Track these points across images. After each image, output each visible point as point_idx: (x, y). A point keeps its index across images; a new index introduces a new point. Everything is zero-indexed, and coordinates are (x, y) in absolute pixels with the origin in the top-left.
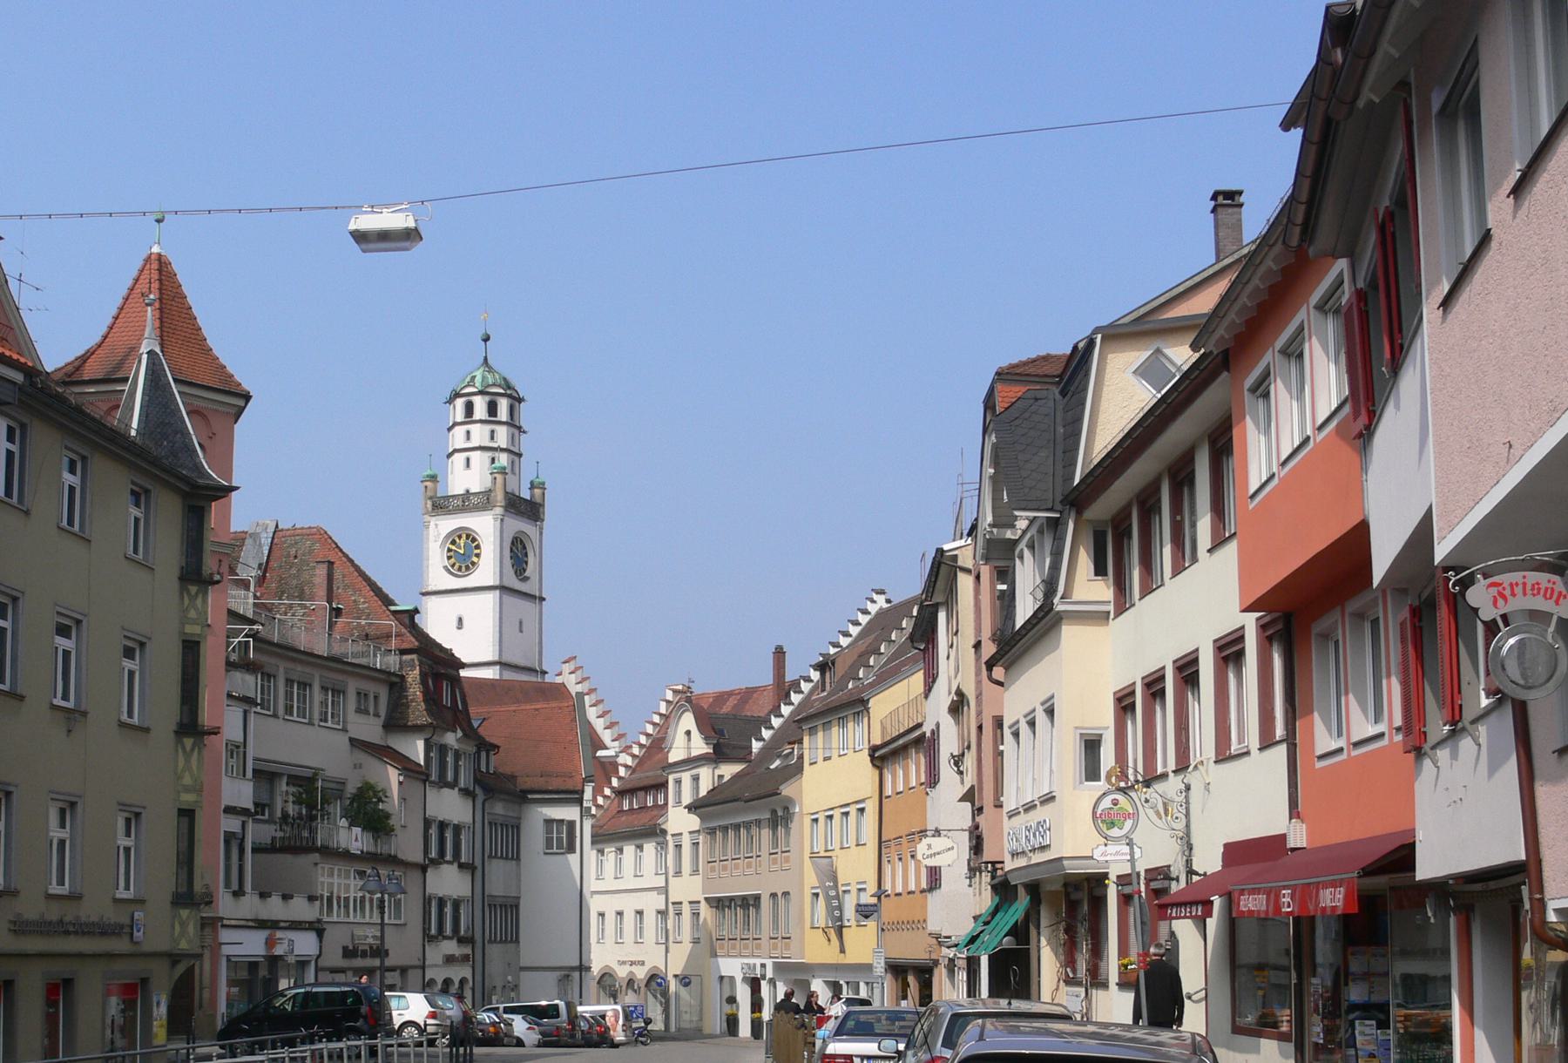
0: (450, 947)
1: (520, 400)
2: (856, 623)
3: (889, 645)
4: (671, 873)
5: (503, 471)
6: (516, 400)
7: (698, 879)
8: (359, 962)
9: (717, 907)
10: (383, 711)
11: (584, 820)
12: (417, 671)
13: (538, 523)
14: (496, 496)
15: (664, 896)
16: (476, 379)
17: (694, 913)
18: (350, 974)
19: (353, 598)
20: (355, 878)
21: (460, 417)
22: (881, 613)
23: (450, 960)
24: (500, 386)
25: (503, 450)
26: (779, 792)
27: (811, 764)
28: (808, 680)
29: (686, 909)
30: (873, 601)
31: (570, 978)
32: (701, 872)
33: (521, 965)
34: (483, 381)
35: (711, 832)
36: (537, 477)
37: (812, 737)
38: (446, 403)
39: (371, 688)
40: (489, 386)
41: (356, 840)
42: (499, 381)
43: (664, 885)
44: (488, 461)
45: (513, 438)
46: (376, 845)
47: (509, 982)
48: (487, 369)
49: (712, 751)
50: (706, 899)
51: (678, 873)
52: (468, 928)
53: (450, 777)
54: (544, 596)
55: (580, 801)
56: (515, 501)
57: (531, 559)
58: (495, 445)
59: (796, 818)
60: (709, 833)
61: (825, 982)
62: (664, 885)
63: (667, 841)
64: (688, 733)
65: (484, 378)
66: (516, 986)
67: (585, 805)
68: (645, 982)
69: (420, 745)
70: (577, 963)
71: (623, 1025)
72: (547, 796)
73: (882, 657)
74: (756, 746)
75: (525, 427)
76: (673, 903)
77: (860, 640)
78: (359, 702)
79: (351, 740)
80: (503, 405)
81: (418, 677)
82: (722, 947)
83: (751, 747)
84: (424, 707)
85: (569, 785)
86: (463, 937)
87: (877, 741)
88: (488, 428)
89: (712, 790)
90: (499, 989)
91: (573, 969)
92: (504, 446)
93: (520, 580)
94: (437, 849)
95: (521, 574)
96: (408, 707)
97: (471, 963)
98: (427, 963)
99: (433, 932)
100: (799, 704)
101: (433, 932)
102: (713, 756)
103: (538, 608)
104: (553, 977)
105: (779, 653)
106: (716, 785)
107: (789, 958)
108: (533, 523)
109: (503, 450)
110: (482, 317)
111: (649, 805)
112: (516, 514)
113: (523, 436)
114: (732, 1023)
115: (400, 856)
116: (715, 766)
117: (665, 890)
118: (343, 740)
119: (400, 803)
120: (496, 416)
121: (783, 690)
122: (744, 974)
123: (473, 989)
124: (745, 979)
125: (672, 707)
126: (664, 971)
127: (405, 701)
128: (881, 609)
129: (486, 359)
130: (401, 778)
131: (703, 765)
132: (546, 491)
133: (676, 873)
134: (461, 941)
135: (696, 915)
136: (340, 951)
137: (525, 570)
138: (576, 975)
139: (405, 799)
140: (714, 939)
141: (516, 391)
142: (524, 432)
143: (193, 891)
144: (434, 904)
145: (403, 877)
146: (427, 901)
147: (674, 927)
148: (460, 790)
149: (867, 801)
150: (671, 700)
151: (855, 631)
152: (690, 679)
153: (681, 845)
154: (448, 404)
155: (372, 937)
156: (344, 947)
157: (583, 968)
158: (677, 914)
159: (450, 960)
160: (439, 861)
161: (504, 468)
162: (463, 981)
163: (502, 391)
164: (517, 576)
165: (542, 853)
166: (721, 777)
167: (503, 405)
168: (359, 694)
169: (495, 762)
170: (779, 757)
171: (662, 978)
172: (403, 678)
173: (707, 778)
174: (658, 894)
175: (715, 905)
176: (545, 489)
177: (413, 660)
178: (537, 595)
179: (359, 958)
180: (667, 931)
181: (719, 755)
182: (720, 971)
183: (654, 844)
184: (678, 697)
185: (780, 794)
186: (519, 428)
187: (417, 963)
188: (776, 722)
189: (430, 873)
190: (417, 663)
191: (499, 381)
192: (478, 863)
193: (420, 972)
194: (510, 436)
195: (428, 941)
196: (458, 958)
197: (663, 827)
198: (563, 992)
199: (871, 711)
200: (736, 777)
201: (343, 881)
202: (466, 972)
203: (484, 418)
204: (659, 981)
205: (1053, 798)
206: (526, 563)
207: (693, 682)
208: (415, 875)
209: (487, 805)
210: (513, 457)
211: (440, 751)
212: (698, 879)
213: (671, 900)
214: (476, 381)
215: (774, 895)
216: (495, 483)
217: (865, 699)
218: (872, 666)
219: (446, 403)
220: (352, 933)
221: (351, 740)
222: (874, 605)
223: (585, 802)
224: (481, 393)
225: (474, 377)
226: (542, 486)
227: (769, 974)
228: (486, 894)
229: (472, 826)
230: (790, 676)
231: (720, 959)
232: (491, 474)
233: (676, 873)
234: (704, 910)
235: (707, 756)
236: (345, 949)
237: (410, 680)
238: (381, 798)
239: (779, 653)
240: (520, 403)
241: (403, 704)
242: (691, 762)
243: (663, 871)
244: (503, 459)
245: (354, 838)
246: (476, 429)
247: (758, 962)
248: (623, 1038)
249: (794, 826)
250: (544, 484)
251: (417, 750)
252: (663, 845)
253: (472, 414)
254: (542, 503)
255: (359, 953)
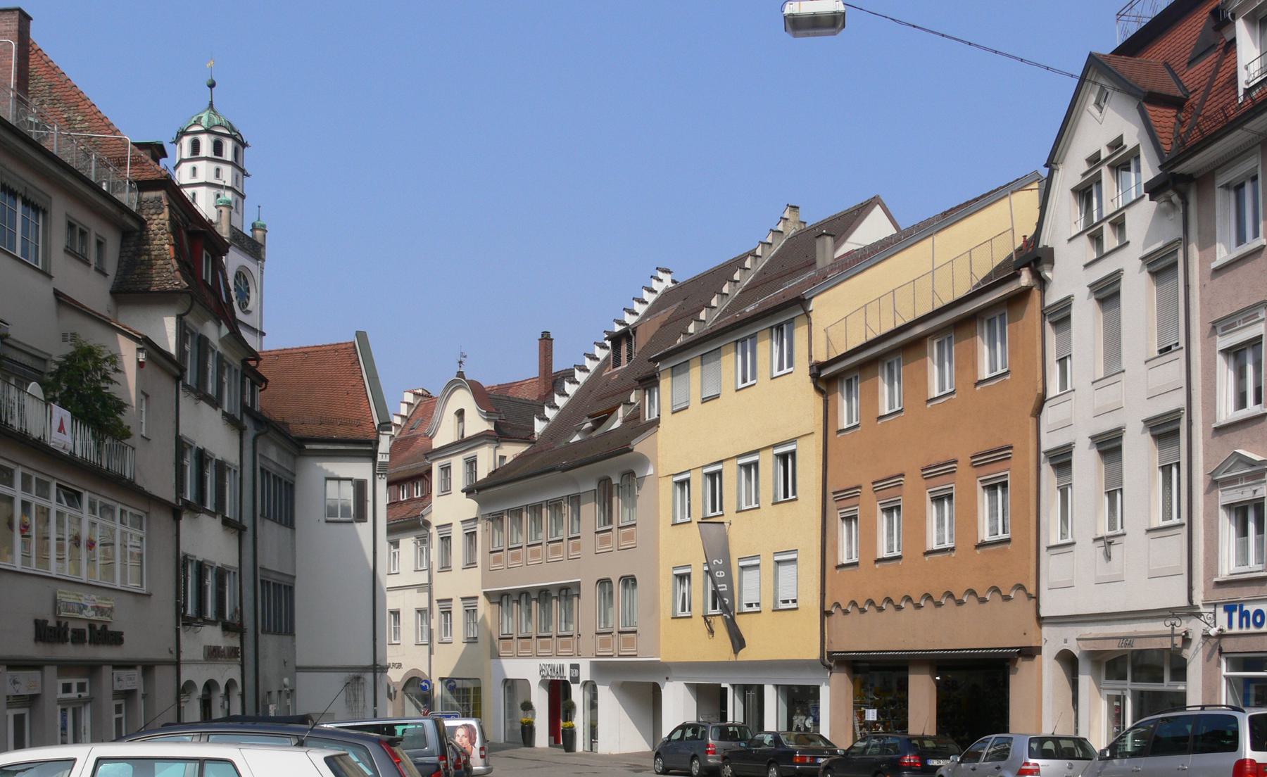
0: (213, 636)
1: (244, 145)
2: (642, 302)
3: (722, 299)
4: (436, 567)
5: (228, 205)
6: (240, 144)
7: (476, 573)
8: (68, 651)
9: (500, 603)
10: (111, 266)
11: (378, 480)
12: (165, 215)
13: (260, 262)
14: (222, 228)
15: (427, 594)
16: (203, 119)
17: (467, 611)
18: (51, 671)
19: (65, 116)
20: (59, 500)
21: (186, 153)
22: (667, 293)
23: (213, 654)
24: (225, 127)
25: (227, 188)
26: (631, 448)
27: (705, 400)
28: (583, 369)
29: (458, 610)
30: (660, 280)
31: (361, 681)
32: (479, 563)
33: (298, 664)
34: (209, 121)
35: (496, 518)
36: (259, 220)
37: (705, 367)
38: (172, 143)
39: (96, 227)
40: (215, 126)
41: (61, 429)
42: (224, 123)
43: (426, 581)
44: (213, 197)
45: (237, 179)
46: (99, 452)
47: (285, 686)
48: (212, 112)
49: (493, 429)
50: (485, 593)
51: (446, 567)
52: (236, 610)
53: (211, 389)
54: (264, 331)
55: (373, 456)
56: (238, 236)
57: (253, 295)
58: (221, 183)
59: (646, 485)
60: (492, 520)
61: (685, 684)
62: (426, 581)
63: (430, 535)
64: (460, 413)
65: (210, 119)
66: (292, 691)
67: (380, 458)
68: (402, 686)
69: (170, 325)
70: (369, 662)
71: (482, 749)
72: (330, 447)
73: (716, 311)
74: (539, 426)
75: (248, 171)
76: (439, 601)
77: (647, 317)
78: (71, 239)
79: (57, 294)
80: (228, 146)
81: (167, 223)
82: (506, 647)
83: (533, 429)
84: (176, 265)
85: (358, 434)
86: (229, 623)
87: (822, 358)
88: (214, 165)
89: (493, 472)
90: (275, 695)
91: (365, 669)
92: (229, 184)
93: (244, 312)
94: (194, 492)
95: (244, 307)
96: (151, 266)
97: (239, 659)
98: (183, 657)
99: (190, 611)
100: (585, 383)
101: (190, 611)
102: (495, 434)
103: (259, 341)
104: (339, 679)
105: (546, 339)
106: (497, 467)
107: (635, 656)
108: (255, 261)
109: (227, 188)
110: (208, 65)
111: (401, 499)
112: (240, 249)
113: (246, 179)
114: (527, 733)
115: (139, 482)
116: (495, 445)
117: (428, 587)
118: (44, 290)
119: (139, 402)
120: (221, 155)
121: (553, 382)
122: (543, 676)
123: (243, 696)
124: (542, 683)
125: (413, 409)
126: (428, 675)
127: (146, 257)
128: (667, 288)
129: (211, 104)
130: (142, 357)
131: (485, 443)
132: (267, 234)
133: (442, 568)
134: (227, 628)
135: (470, 612)
136: (30, 631)
137: (247, 305)
138: (369, 677)
139: (147, 396)
140: (496, 638)
141: (240, 134)
142: (248, 176)
143: (223, 718)
144: (191, 571)
145: (144, 518)
146: (181, 563)
147: (440, 626)
148: (224, 414)
149: (798, 441)
150: (412, 402)
151: (641, 309)
152: (462, 353)
153: (449, 537)
154: (174, 144)
155: (93, 608)
156: (37, 622)
157: (378, 668)
158: (443, 612)
159: (213, 654)
160: (197, 507)
161: (229, 202)
162: (230, 685)
163: (227, 132)
164: (241, 309)
165: (323, 520)
166: (503, 458)
167: (228, 146)
168: (71, 226)
169: (262, 401)
170: (578, 431)
171: (426, 681)
172: (143, 223)
173: (486, 460)
174: (418, 592)
175: (498, 600)
176: (267, 231)
177: (159, 199)
178: (258, 329)
179: (69, 643)
180: (430, 631)
181: (499, 435)
182: (505, 675)
183: (414, 538)
184: (419, 400)
185: (632, 450)
186: (243, 171)
187: (168, 656)
188: (550, 413)
189: (185, 522)
190: (165, 203)
191: (224, 123)
192: (247, 522)
193: (171, 671)
194: (235, 177)
195: (183, 624)
196: (223, 651)
197: (426, 518)
198: (352, 697)
199: (812, 315)
200: (520, 459)
201: (35, 501)
202: (234, 672)
203: (209, 156)
204: (423, 684)
205: (904, 475)
206: (248, 298)
207: (465, 357)
208: (162, 521)
209: (259, 444)
210: (237, 196)
211: (199, 345)
212: (476, 573)
213: (436, 596)
214: (202, 121)
215: (604, 583)
216: (221, 216)
217: (807, 298)
218: (704, 321)
219: (172, 143)
220: (55, 597)
221: (57, 294)
222: (660, 283)
223: (379, 456)
224: (207, 131)
225: (200, 118)
226: (264, 230)
227: (585, 675)
228: (259, 565)
229: (239, 470)
230: (557, 367)
231: (504, 661)
232: (216, 207)
233: (442, 568)
234: (483, 607)
235: (488, 433)
236: (40, 626)
237: (153, 227)
238: (106, 373)
239: (546, 339)
240: (244, 148)
241: (142, 262)
242: (465, 443)
243: (425, 567)
244: (228, 195)
245: (56, 425)
246: (202, 166)
247: (567, 663)
248: (481, 768)
249: (643, 495)
250: (264, 226)
251: (166, 331)
252: (424, 540)
253: (199, 151)
254: (263, 244)
255: (70, 634)
